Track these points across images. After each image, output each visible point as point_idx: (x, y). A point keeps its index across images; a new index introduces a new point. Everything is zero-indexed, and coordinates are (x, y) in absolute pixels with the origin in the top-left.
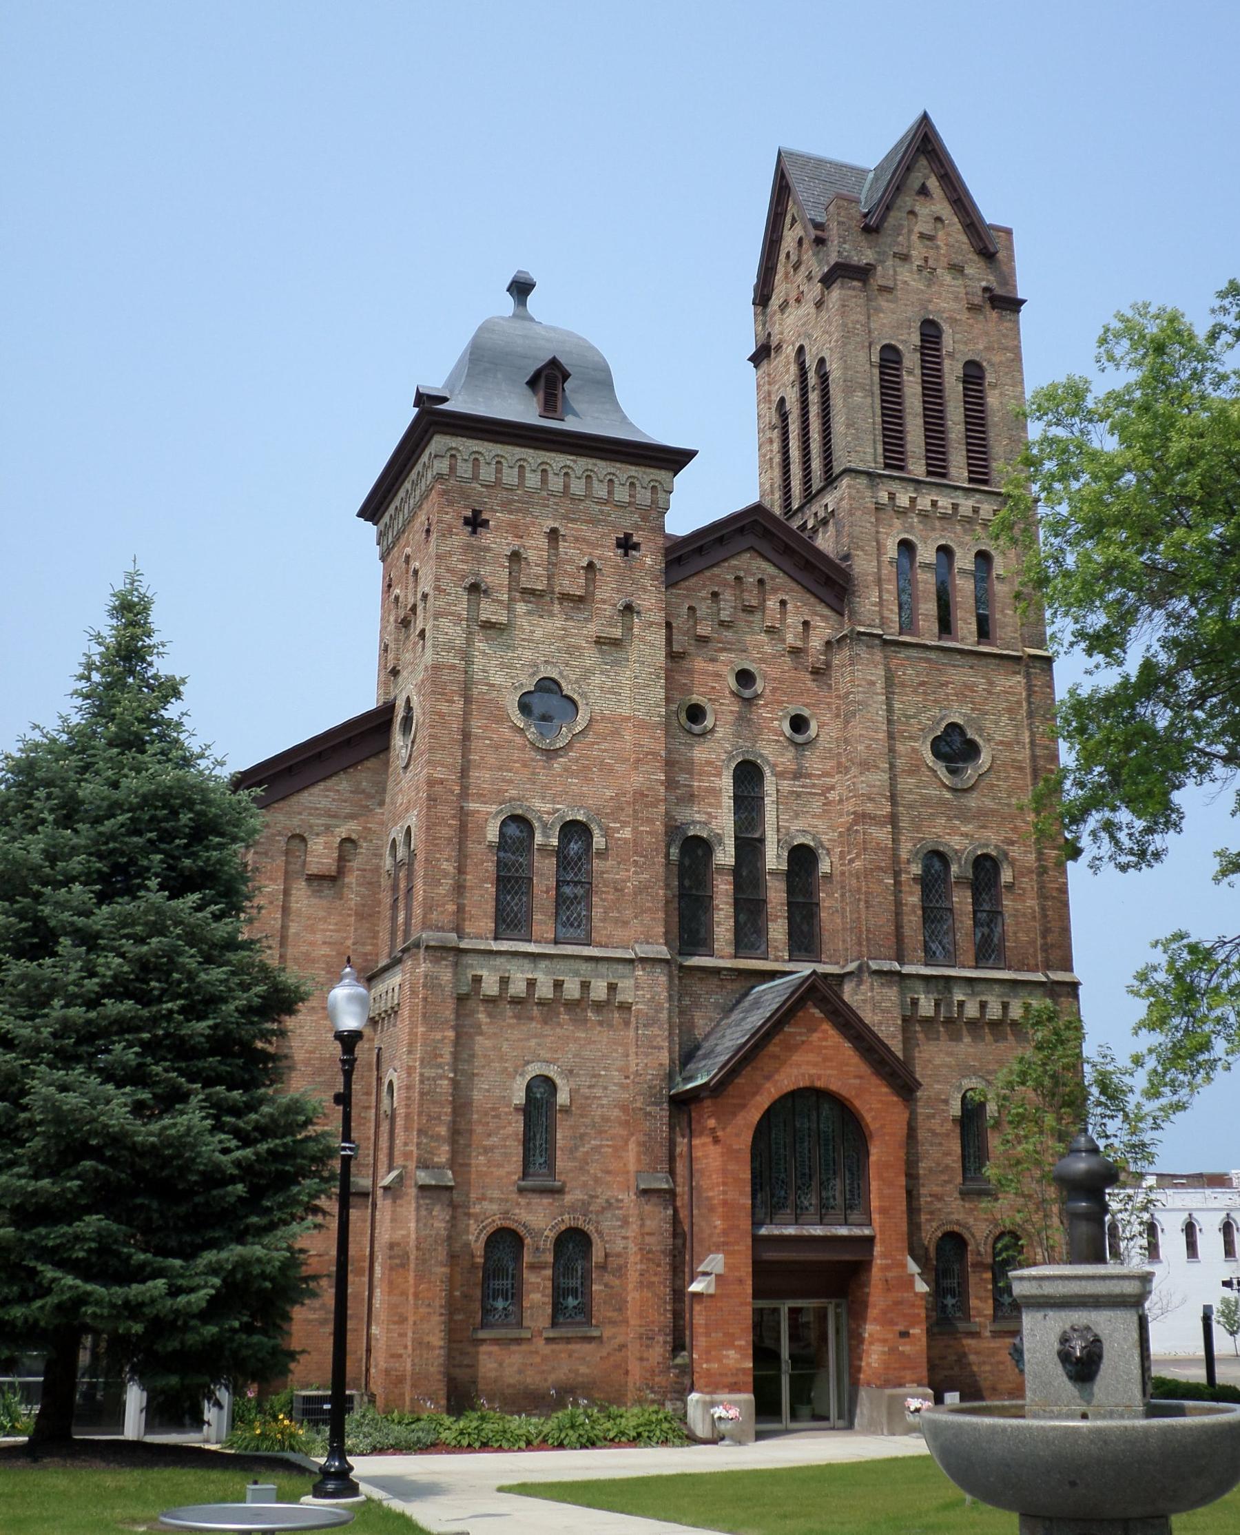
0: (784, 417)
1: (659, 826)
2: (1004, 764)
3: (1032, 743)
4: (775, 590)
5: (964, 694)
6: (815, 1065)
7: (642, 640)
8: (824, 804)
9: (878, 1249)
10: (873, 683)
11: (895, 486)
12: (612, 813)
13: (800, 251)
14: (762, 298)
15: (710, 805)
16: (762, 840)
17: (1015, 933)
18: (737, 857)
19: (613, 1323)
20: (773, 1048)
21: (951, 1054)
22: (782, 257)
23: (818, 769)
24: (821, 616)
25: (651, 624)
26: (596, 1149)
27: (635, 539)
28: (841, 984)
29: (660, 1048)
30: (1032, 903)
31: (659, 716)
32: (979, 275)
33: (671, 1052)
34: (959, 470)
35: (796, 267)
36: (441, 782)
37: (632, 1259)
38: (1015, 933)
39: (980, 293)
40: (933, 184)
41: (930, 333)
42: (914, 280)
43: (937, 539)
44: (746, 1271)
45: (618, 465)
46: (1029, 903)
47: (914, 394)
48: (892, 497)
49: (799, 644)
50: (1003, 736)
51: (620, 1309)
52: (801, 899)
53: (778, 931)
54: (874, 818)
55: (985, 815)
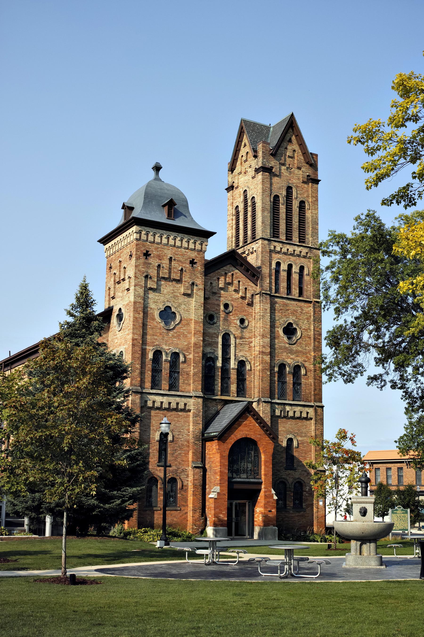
0: (238, 213)
1: (201, 354)
2: (305, 336)
3: (314, 330)
4: (237, 278)
5: (294, 312)
6: (248, 431)
7: (197, 294)
8: (249, 347)
9: (263, 486)
10: (266, 309)
11: (276, 244)
12: (186, 350)
13: (247, 156)
14: (232, 169)
15: (215, 347)
16: (230, 358)
17: (305, 390)
18: (222, 364)
19: (184, 506)
20: (235, 426)
21: (284, 427)
22: (240, 156)
23: (248, 336)
24: (251, 286)
25: (200, 289)
26: (180, 454)
27: (195, 261)
28: (252, 404)
29: (199, 424)
30: (311, 381)
31: (201, 319)
32: (306, 170)
33: (202, 425)
34: (296, 239)
35: (246, 161)
36: (136, 339)
37: (189, 487)
38: (305, 390)
39: (306, 177)
40: (293, 138)
41: (289, 189)
42: (285, 172)
43: (288, 262)
44: (226, 492)
45: (191, 236)
46: (310, 380)
47: (284, 212)
48: (275, 247)
49: (244, 295)
50: (305, 327)
51: (186, 502)
52: (241, 378)
53: (233, 387)
54: (265, 353)
55: (298, 352)
